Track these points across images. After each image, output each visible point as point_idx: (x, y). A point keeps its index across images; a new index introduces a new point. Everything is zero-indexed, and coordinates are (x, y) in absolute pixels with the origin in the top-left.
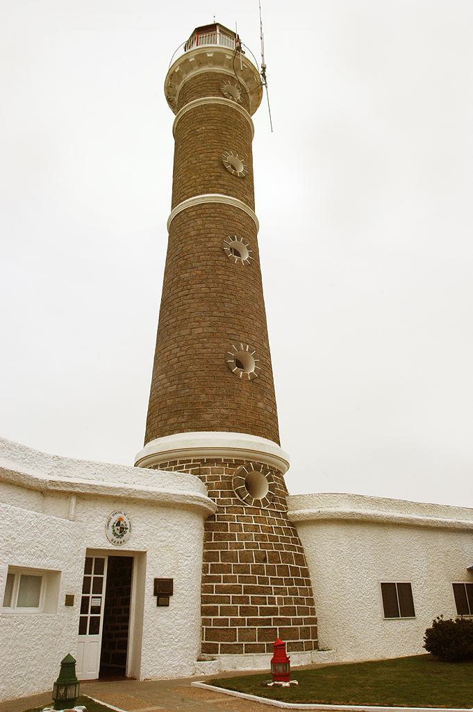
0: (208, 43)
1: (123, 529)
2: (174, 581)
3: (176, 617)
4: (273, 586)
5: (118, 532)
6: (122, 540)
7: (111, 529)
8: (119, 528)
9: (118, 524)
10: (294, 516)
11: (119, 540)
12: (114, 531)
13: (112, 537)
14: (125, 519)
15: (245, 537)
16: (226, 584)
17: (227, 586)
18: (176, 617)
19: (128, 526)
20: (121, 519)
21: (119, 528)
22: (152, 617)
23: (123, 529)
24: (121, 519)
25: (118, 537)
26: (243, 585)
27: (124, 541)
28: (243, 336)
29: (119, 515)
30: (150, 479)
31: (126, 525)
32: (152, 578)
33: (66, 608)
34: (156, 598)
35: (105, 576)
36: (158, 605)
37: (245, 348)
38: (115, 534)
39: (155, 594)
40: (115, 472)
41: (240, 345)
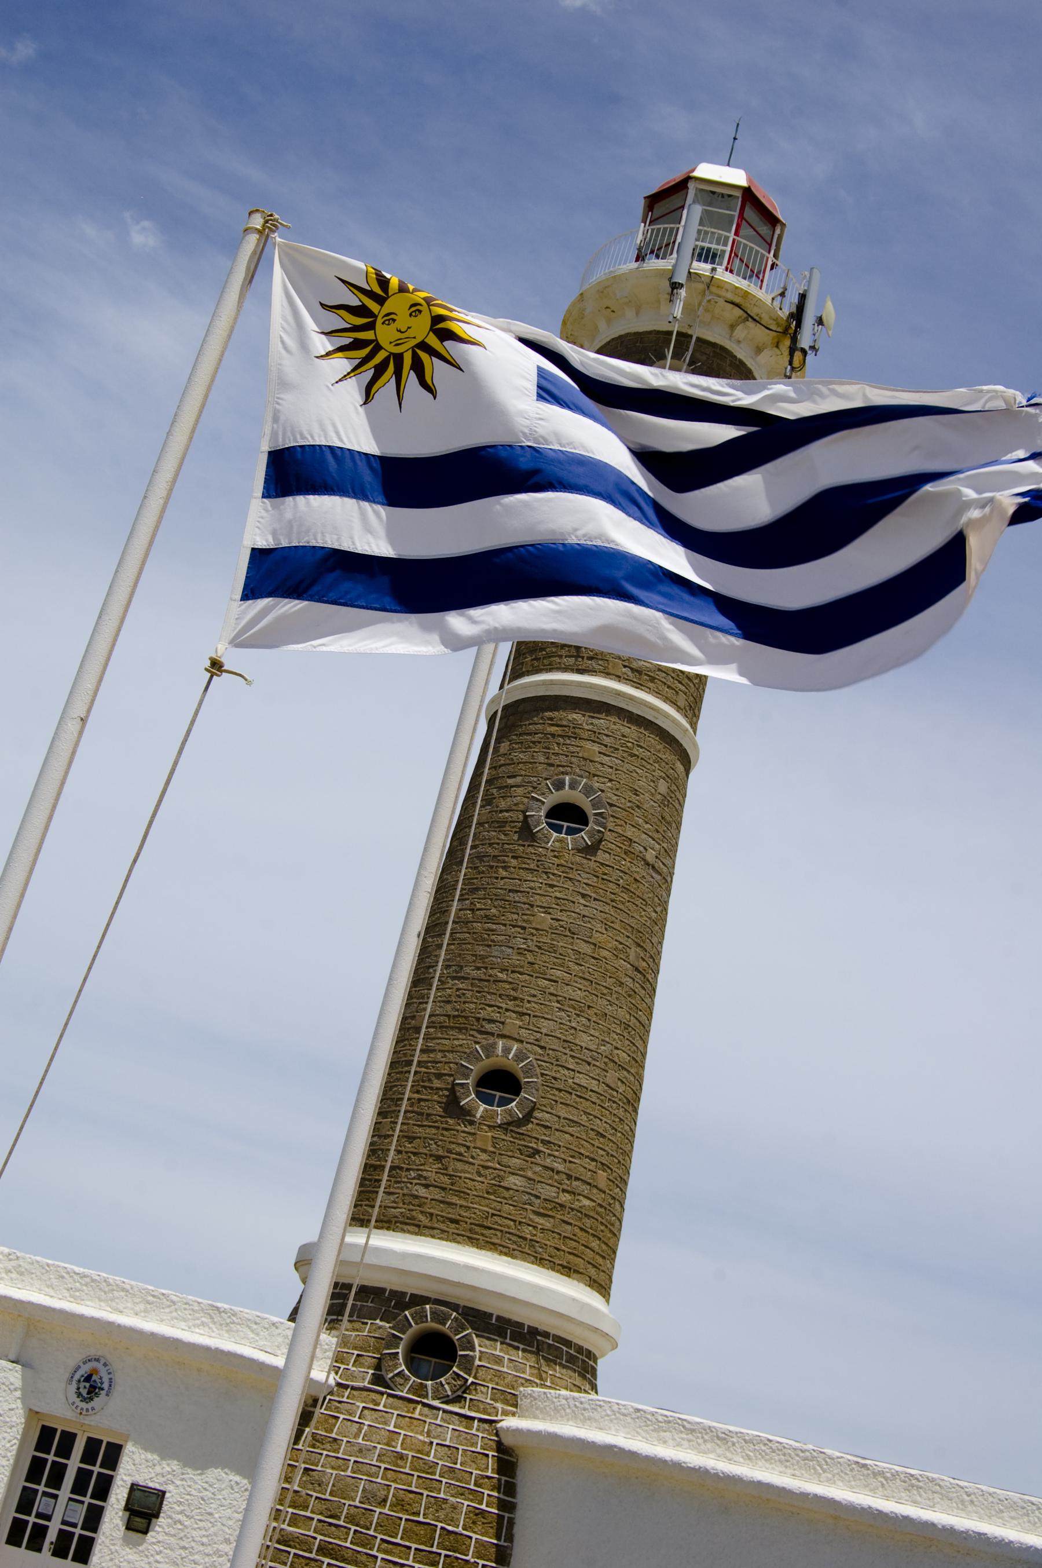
0: (702, 249)
1: (95, 1388)
2: (167, 1495)
3: (158, 1557)
4: (380, 1556)
5: (84, 1392)
6: (90, 1405)
7: (74, 1385)
8: (87, 1385)
9: (88, 1378)
10: (508, 1429)
11: (83, 1405)
12: (78, 1389)
13: (73, 1397)
14: (103, 1372)
15: (360, 1451)
16: (291, 1529)
17: (291, 1533)
18: (158, 1557)
19: (106, 1386)
20: (95, 1371)
21: (87, 1385)
22: (114, 1545)
23: (95, 1388)
24: (95, 1371)
25: (84, 1400)
26: (320, 1537)
27: (93, 1409)
28: (513, 1022)
29: (94, 1364)
30: (167, 1310)
31: (102, 1383)
32: (129, 1481)
33: (126, 1542)
34: (127, 1514)
35: (566, 824)
36: (129, 1527)
37: (507, 1050)
38: (79, 1395)
39: (127, 1508)
40: (107, 1289)
41: (494, 1046)
